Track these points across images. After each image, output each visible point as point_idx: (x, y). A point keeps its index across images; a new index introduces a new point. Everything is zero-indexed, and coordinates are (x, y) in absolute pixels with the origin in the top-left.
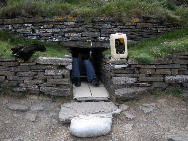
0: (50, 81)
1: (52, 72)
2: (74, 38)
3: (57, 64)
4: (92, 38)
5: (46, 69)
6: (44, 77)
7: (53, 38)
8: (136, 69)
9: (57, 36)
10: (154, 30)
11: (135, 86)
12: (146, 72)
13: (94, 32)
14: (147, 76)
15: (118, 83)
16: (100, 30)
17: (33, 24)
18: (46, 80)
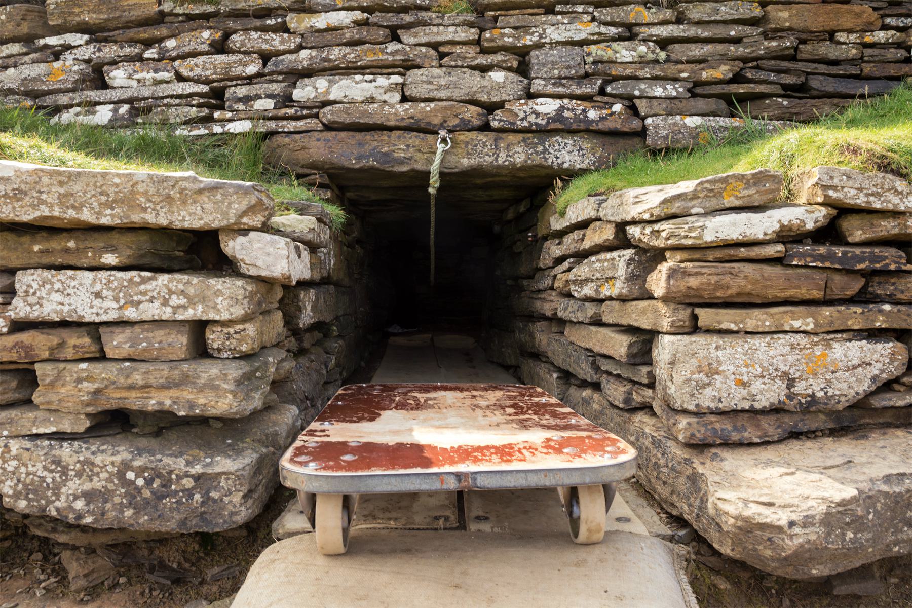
9: (247, 100)
10: (885, 45)
13: (484, 69)
15: (725, 392)
16: (523, 54)
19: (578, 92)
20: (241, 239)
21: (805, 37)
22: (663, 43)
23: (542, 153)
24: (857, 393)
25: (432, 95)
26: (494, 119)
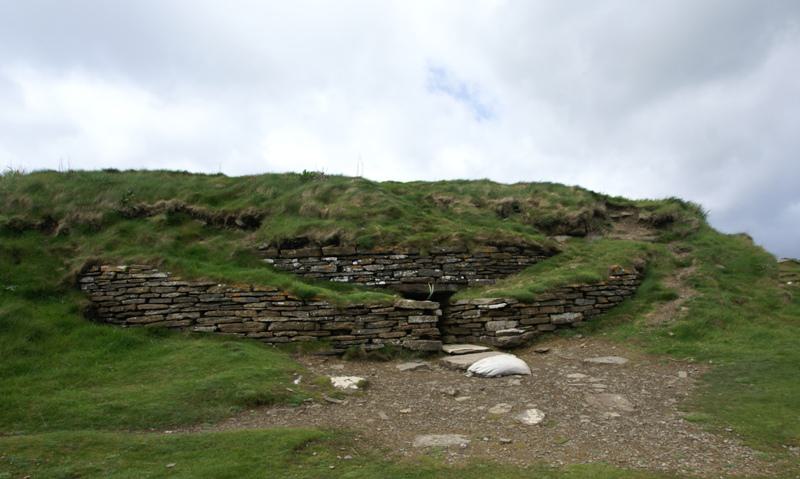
1: (418, 319)
17: (340, 257)
21: (498, 260)
22: (470, 263)
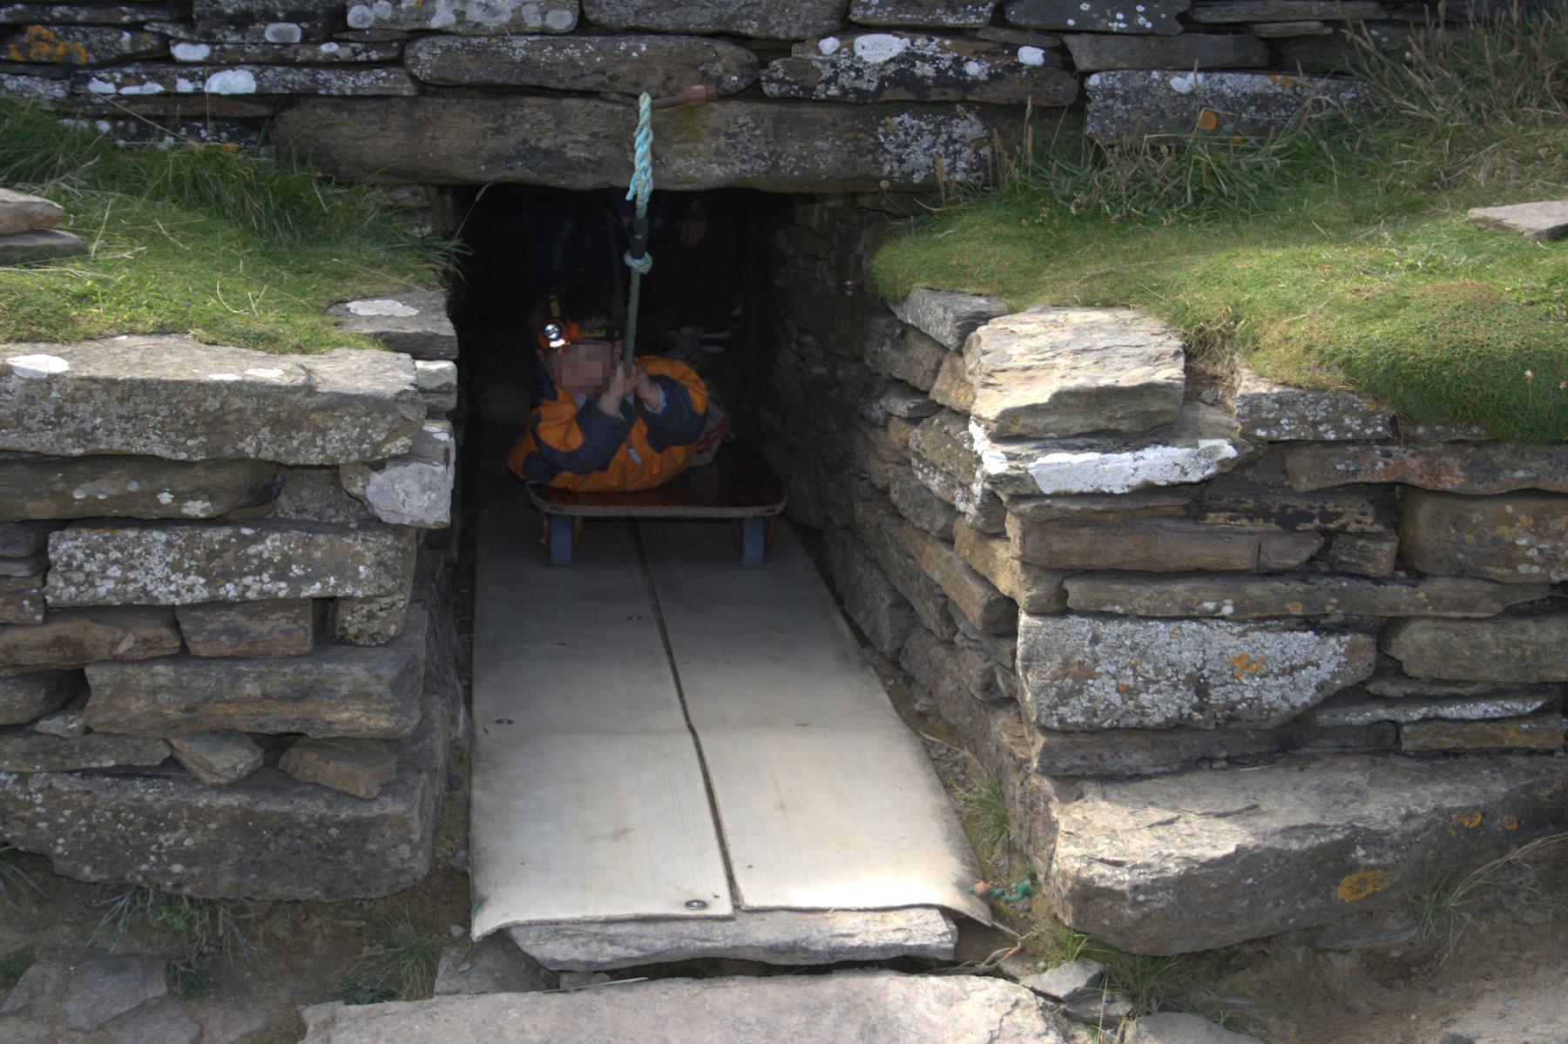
0: (137, 693)
1: (159, 571)
2: (479, 53)
3: (228, 450)
4: (721, 47)
5: (63, 524)
6: (32, 640)
7: (182, 52)
8: (1357, 516)
11: (1343, 751)
12: (1510, 556)
14: (1515, 612)
18: (68, 687)
19: (951, 21)
20: (377, 478)
23: (870, 151)
24: (1294, 707)
25: (643, 22)
26: (770, 80)
